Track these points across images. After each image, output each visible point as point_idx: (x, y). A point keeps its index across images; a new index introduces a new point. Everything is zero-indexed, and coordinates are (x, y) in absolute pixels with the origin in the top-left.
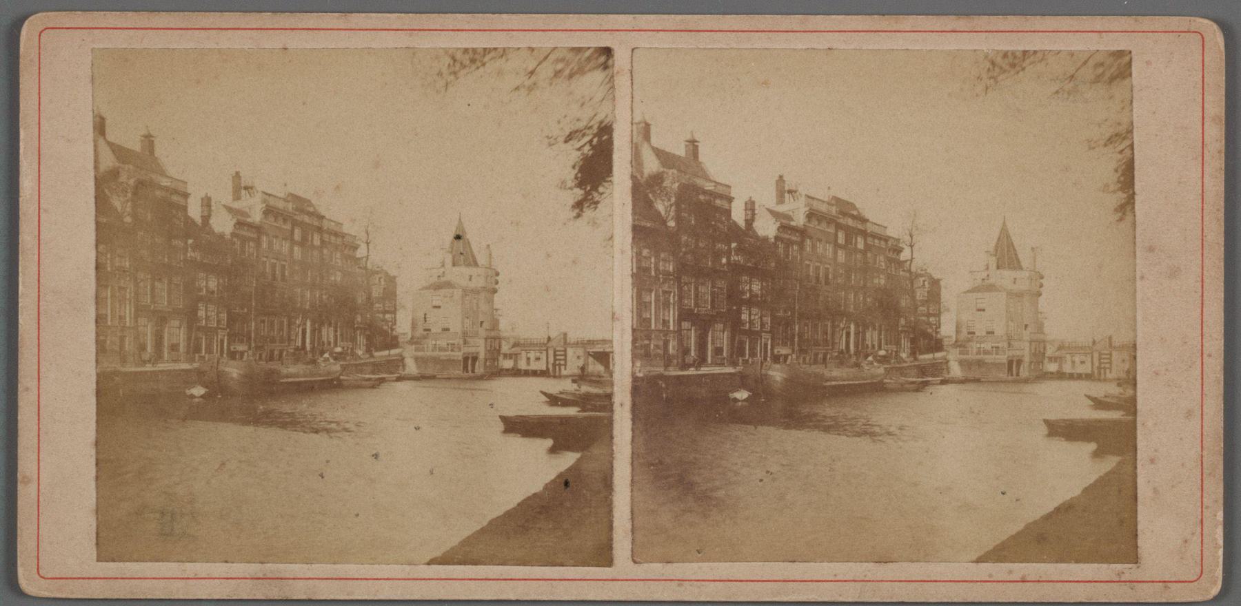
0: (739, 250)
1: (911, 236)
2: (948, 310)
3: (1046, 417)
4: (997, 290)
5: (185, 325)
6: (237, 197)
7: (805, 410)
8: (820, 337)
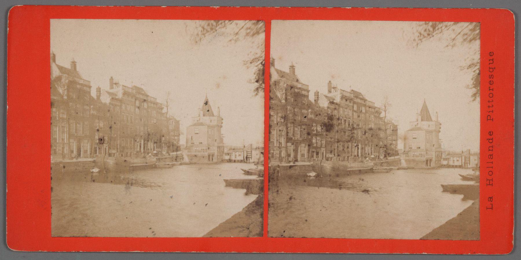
1: (385, 107)
2: (183, 134)
3: (224, 179)
6: (112, 88)
7: (340, 180)
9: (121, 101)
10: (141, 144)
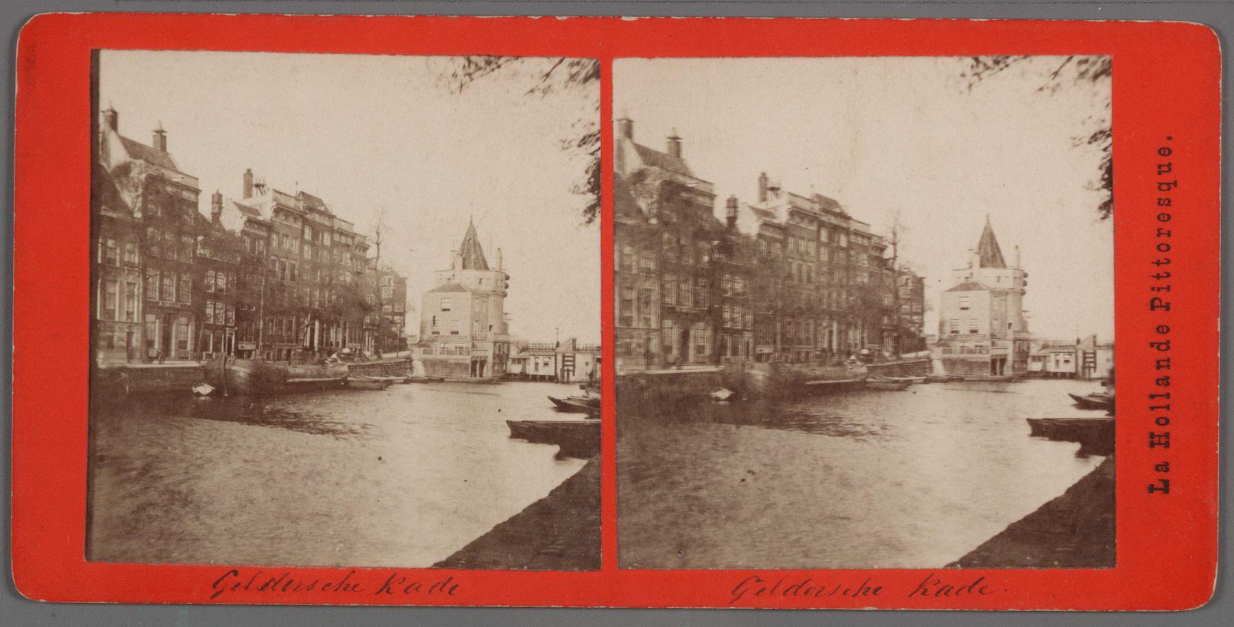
0: (205, 244)
1: (894, 234)
4: (981, 289)
5: (193, 323)
6: (248, 194)
8: (802, 335)
9: (269, 227)
10: (831, 332)
